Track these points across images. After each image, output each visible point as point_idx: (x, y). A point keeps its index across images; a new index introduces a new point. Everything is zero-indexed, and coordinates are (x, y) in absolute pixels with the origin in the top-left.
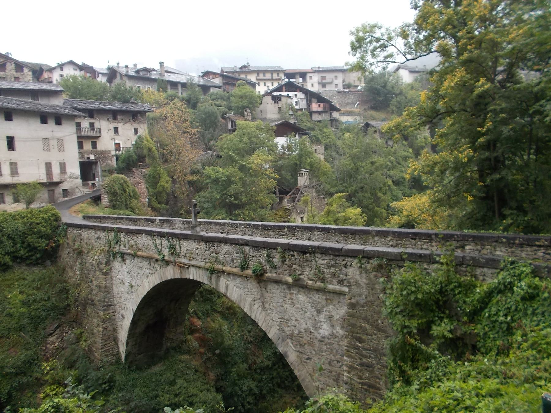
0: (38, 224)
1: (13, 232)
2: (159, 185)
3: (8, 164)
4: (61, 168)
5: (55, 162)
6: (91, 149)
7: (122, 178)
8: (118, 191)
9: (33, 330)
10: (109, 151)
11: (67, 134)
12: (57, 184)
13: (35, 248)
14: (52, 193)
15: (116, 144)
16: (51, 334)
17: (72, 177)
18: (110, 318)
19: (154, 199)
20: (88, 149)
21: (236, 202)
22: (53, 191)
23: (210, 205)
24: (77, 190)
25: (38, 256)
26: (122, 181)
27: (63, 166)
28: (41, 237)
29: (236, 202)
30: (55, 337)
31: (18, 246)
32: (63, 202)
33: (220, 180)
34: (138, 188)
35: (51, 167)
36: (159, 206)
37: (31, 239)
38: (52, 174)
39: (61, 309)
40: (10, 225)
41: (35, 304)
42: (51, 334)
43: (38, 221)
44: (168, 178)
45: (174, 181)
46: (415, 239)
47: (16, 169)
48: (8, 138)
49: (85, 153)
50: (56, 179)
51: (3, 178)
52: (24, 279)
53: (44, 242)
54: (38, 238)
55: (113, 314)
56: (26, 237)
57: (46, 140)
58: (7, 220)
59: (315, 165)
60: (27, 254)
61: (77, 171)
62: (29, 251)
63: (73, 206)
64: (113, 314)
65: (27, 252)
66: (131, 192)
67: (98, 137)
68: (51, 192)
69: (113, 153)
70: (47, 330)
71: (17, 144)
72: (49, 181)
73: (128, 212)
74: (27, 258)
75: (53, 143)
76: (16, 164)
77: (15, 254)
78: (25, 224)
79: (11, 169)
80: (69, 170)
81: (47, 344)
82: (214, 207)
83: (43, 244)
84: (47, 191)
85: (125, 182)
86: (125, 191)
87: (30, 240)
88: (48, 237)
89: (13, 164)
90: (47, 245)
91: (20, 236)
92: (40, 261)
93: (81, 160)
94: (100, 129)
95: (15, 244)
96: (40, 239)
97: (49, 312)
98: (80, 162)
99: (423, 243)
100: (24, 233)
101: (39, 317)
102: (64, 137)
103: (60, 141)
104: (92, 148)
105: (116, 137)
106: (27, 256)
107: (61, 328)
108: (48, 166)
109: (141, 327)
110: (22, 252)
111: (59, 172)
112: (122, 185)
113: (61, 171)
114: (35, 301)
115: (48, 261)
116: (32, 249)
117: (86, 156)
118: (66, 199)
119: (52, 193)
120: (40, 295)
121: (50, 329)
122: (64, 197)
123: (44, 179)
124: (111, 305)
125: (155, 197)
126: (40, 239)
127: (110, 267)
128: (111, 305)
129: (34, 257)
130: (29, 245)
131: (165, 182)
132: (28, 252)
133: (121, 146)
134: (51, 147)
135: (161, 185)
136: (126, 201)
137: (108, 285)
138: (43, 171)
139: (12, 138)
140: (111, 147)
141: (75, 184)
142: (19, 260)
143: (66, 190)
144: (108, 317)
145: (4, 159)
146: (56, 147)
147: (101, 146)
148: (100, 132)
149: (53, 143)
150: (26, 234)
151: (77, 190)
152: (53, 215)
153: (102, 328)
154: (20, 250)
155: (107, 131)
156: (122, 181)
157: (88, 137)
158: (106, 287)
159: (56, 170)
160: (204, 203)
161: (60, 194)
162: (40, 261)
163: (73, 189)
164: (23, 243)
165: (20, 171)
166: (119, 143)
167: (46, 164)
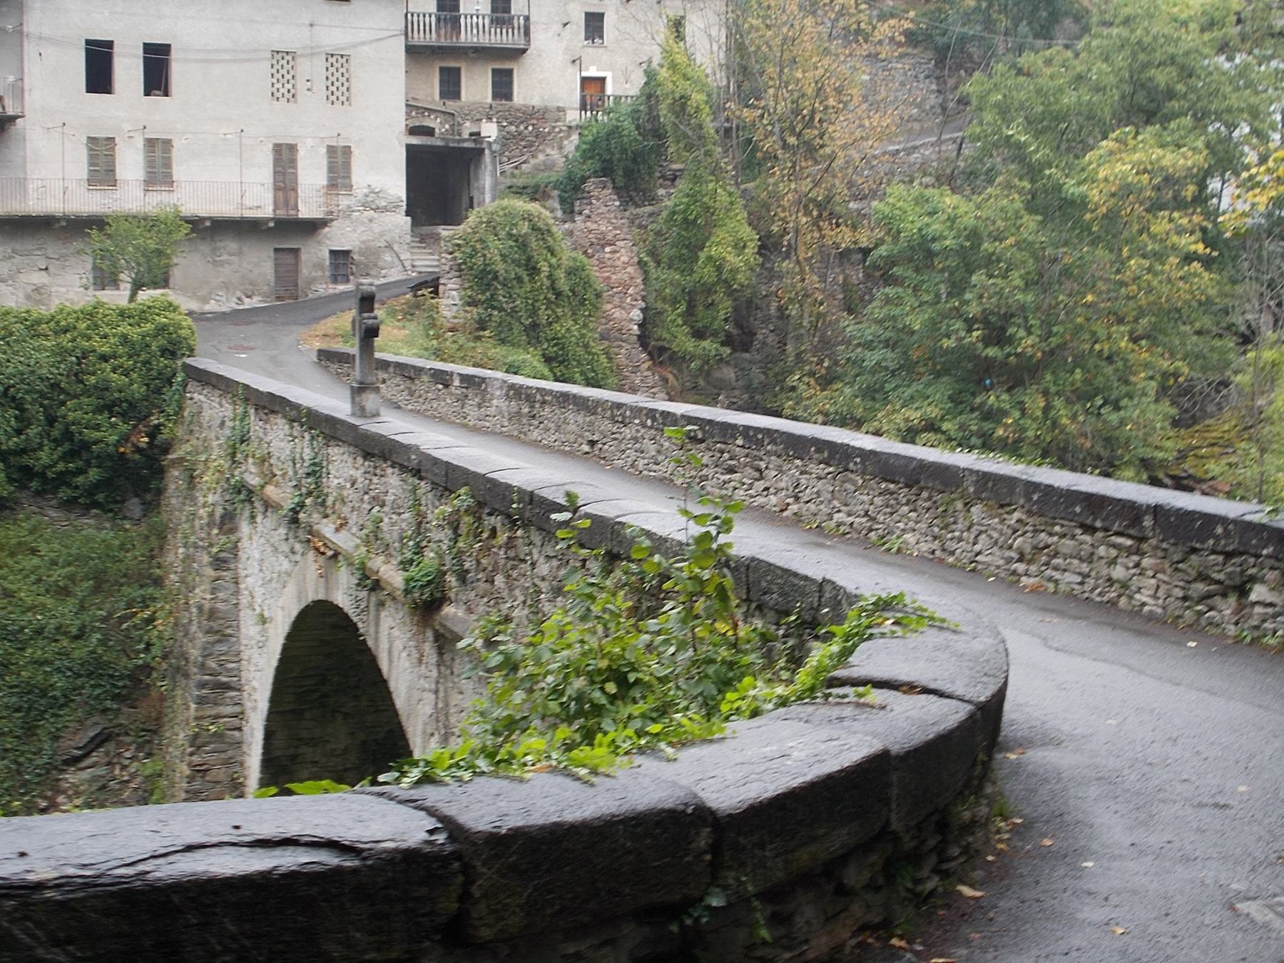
0: (104, 358)
1: (22, 381)
2: (703, 255)
3: (140, 143)
4: (332, 169)
5: (309, 142)
6: (489, 100)
7: (528, 217)
8: (500, 267)
9: (19, 732)
10: (560, 109)
11: (364, 35)
12: (312, 227)
13: (86, 445)
14: (288, 260)
15: (585, 81)
16: (77, 760)
17: (373, 204)
18: (218, 736)
19: (674, 315)
20: (478, 98)
21: (992, 352)
22: (296, 252)
23: (890, 358)
24: (388, 257)
25: (94, 474)
26: (525, 228)
27: (339, 163)
28: (109, 408)
29: (992, 352)
30: (86, 775)
31: (33, 431)
32: (335, 295)
33: (936, 246)
34: (601, 261)
35: (293, 162)
36: (690, 345)
37: (73, 412)
38: (295, 190)
39: (122, 677)
40: (16, 353)
41: (41, 643)
42: (75, 761)
43: (105, 349)
44: (747, 232)
45: (768, 246)
46: (1089, 529)
47: (168, 164)
48: (148, 48)
49: (465, 116)
50: (306, 211)
51: (117, 195)
52: (34, 551)
53: (113, 426)
54: (99, 410)
55: (235, 722)
56: (63, 403)
57: (283, 57)
58: (11, 334)
59: (625, 132)
60: (61, 466)
61: (395, 185)
62: (70, 455)
63: (325, 317)
64: (235, 722)
65: (63, 458)
66: (560, 274)
67: (518, 53)
68: (289, 259)
69: (573, 116)
70: (64, 743)
71: (178, 72)
72: (281, 213)
73: (531, 358)
74: (63, 479)
75: (312, 70)
76: (167, 143)
77: (25, 460)
78: (62, 353)
79: (150, 163)
80: (363, 177)
81: (60, 791)
82: (908, 368)
83: (109, 433)
84: (272, 254)
85: (542, 232)
86: (534, 271)
87: (71, 416)
88: (130, 410)
89: (159, 147)
90: (125, 438)
91: (42, 395)
92: (100, 497)
93: (415, 140)
94: (527, 19)
95: (24, 421)
96: (106, 415)
97: (79, 682)
98: (410, 149)
99: (1114, 552)
100: (55, 386)
101: (43, 693)
102: (355, 46)
103: (338, 60)
104: (495, 96)
105: (590, 52)
106: (61, 473)
107: (111, 746)
108: (285, 157)
109: (525, 833)
110: (44, 456)
111: (325, 182)
112: (522, 244)
113: (330, 179)
114: (39, 632)
115: (135, 500)
116: (77, 449)
117: (468, 128)
118: (341, 288)
119: (288, 260)
120: (65, 612)
121: (73, 742)
122: (335, 280)
123: (261, 204)
124: (227, 687)
125: (683, 308)
126: (106, 415)
127: (233, 538)
128: (227, 687)
129: (80, 480)
130: (68, 435)
131: (731, 247)
132: (66, 457)
133: (609, 90)
134: (302, 85)
135: (710, 258)
136: (534, 312)
137: (219, 606)
138: (265, 174)
139: (164, 49)
140: (567, 94)
141: (382, 234)
142: (34, 484)
143: (347, 253)
144: (213, 728)
145: (127, 127)
146: (320, 85)
147: (526, 92)
148: (527, 33)
149: (312, 70)
150: (63, 391)
151: (388, 257)
152: (162, 329)
153: (189, 764)
154: (41, 447)
155: (557, 27)
156: (525, 228)
157: (481, 53)
158: (212, 614)
159: (312, 173)
160: (869, 346)
161: (319, 266)
162: (100, 497)
163: (373, 253)
164: (51, 421)
165: (178, 172)
166: (602, 80)
167: (278, 149)
